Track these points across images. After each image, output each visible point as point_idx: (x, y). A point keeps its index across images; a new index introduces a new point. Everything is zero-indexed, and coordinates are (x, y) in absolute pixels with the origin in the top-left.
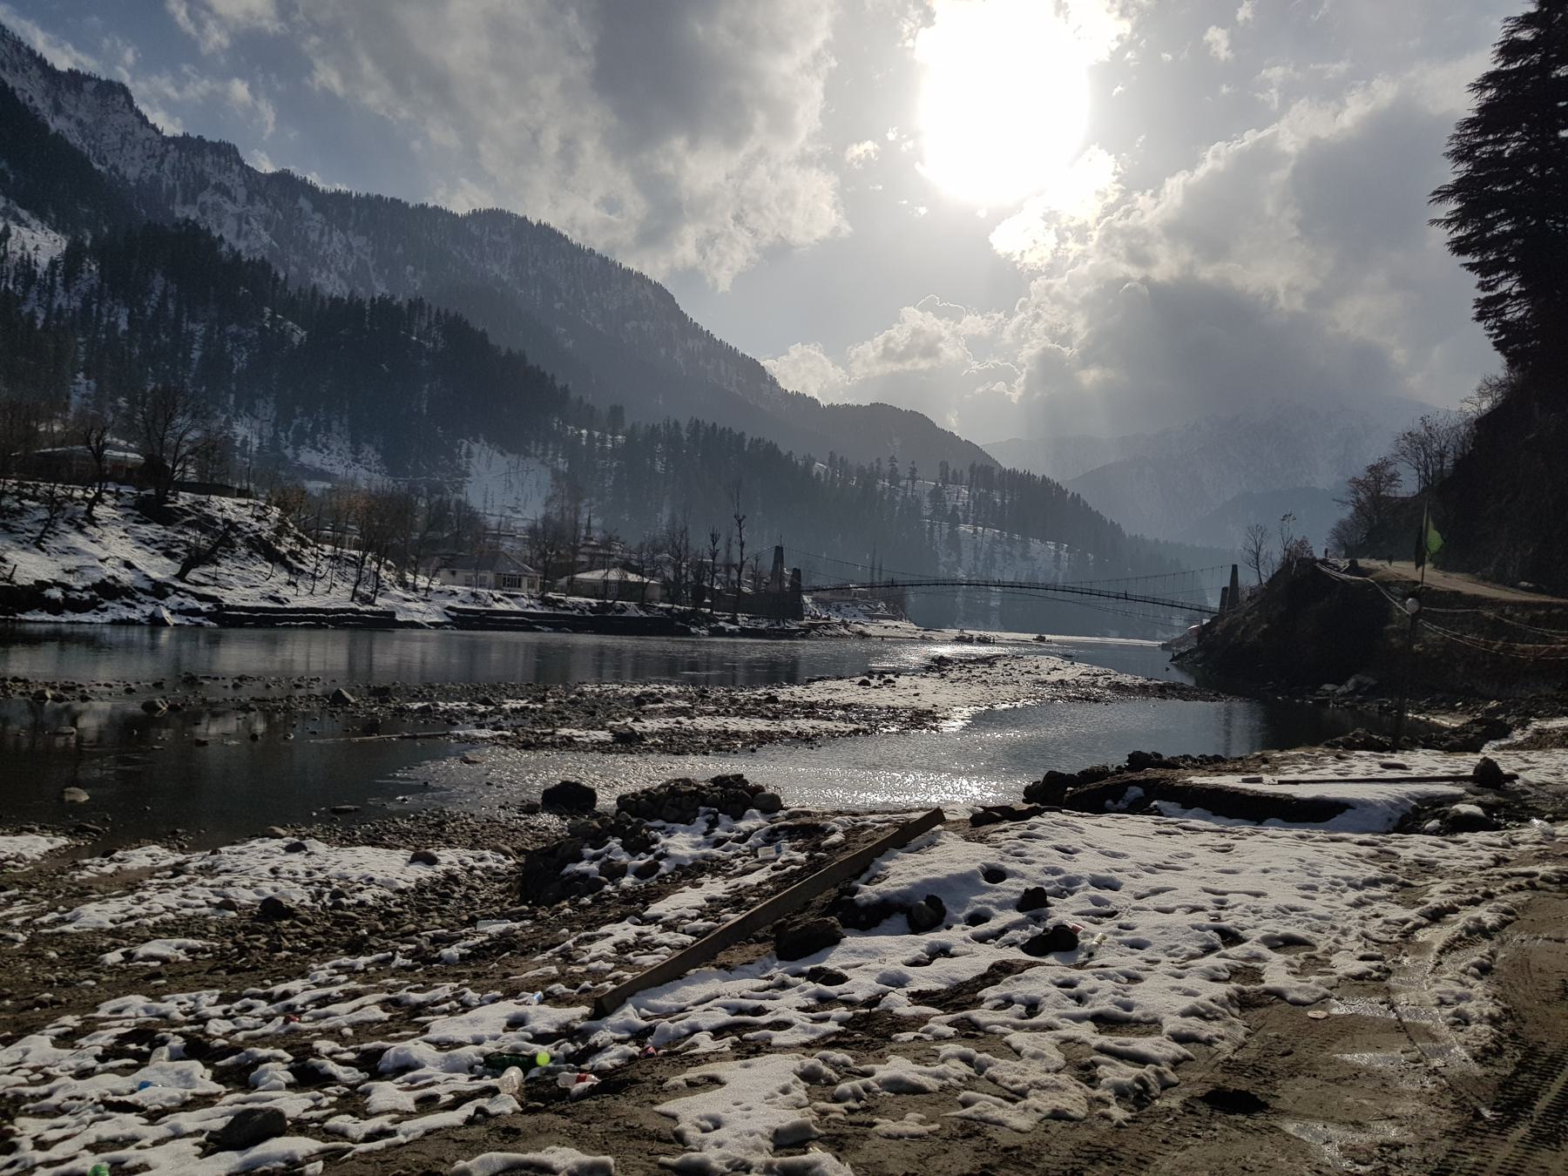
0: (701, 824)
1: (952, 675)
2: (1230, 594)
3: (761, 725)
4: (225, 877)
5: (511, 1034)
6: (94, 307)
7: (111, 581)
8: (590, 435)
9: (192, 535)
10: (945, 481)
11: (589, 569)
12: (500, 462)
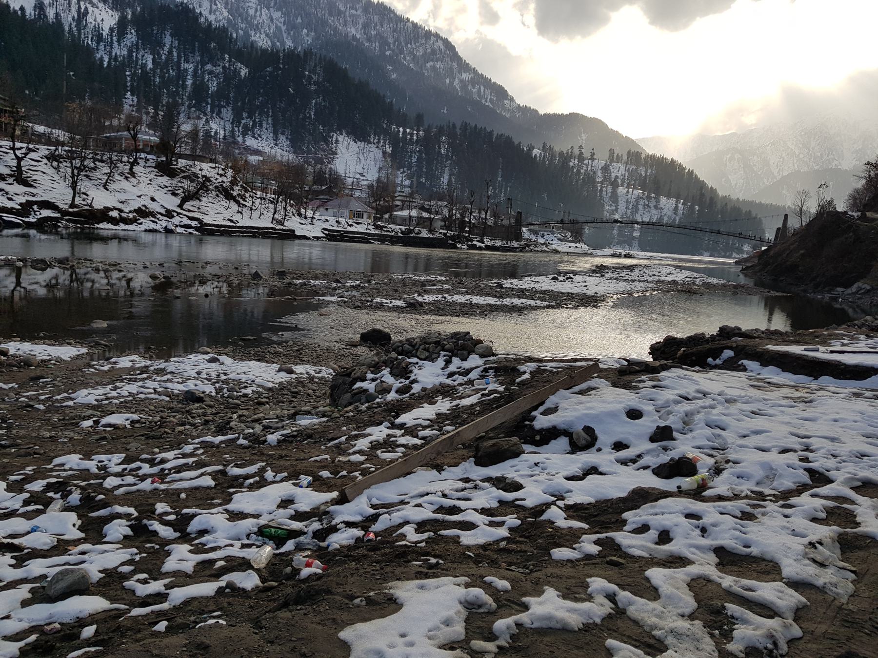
0: (441, 362)
1: (608, 276)
2: (781, 232)
3: (492, 301)
4: (169, 377)
5: (281, 510)
6: (134, 54)
7: (144, 208)
8: (404, 132)
9: (186, 184)
10: (612, 161)
11: (402, 209)
12: (354, 146)
